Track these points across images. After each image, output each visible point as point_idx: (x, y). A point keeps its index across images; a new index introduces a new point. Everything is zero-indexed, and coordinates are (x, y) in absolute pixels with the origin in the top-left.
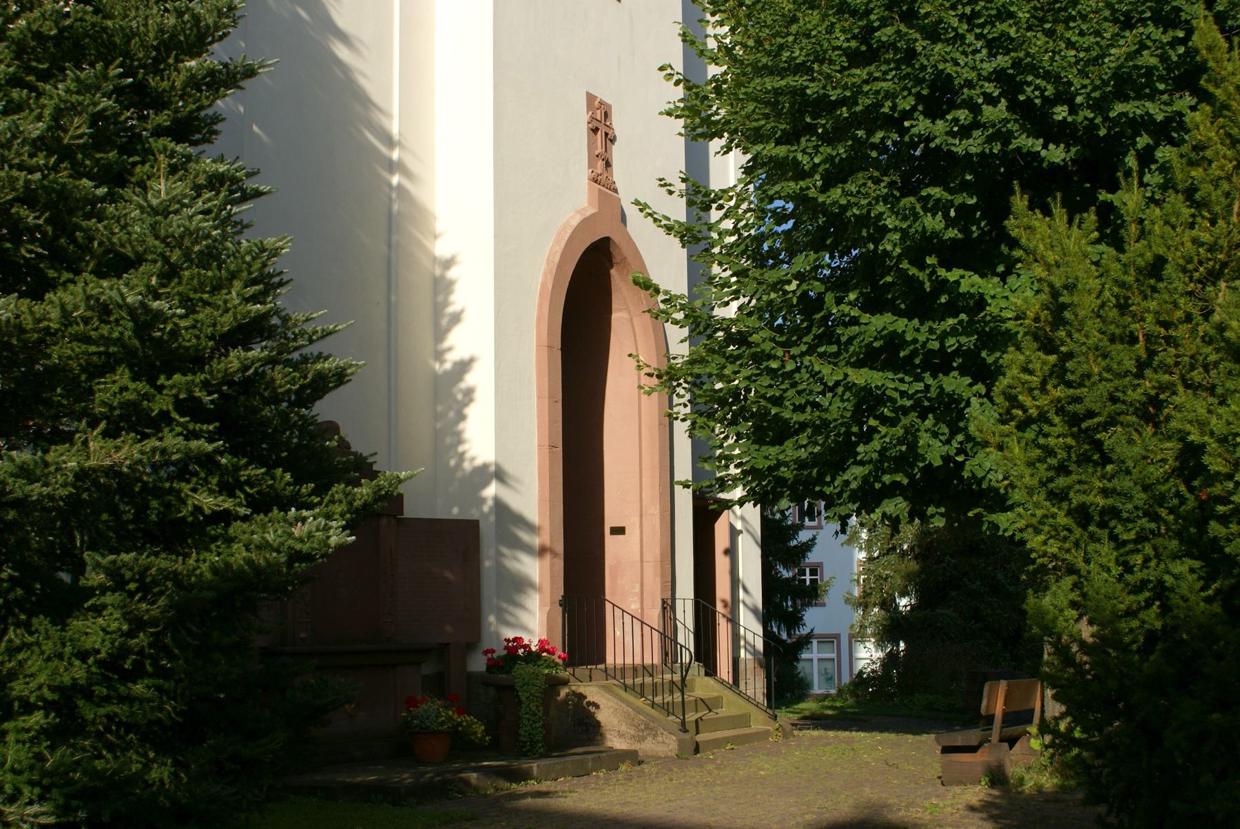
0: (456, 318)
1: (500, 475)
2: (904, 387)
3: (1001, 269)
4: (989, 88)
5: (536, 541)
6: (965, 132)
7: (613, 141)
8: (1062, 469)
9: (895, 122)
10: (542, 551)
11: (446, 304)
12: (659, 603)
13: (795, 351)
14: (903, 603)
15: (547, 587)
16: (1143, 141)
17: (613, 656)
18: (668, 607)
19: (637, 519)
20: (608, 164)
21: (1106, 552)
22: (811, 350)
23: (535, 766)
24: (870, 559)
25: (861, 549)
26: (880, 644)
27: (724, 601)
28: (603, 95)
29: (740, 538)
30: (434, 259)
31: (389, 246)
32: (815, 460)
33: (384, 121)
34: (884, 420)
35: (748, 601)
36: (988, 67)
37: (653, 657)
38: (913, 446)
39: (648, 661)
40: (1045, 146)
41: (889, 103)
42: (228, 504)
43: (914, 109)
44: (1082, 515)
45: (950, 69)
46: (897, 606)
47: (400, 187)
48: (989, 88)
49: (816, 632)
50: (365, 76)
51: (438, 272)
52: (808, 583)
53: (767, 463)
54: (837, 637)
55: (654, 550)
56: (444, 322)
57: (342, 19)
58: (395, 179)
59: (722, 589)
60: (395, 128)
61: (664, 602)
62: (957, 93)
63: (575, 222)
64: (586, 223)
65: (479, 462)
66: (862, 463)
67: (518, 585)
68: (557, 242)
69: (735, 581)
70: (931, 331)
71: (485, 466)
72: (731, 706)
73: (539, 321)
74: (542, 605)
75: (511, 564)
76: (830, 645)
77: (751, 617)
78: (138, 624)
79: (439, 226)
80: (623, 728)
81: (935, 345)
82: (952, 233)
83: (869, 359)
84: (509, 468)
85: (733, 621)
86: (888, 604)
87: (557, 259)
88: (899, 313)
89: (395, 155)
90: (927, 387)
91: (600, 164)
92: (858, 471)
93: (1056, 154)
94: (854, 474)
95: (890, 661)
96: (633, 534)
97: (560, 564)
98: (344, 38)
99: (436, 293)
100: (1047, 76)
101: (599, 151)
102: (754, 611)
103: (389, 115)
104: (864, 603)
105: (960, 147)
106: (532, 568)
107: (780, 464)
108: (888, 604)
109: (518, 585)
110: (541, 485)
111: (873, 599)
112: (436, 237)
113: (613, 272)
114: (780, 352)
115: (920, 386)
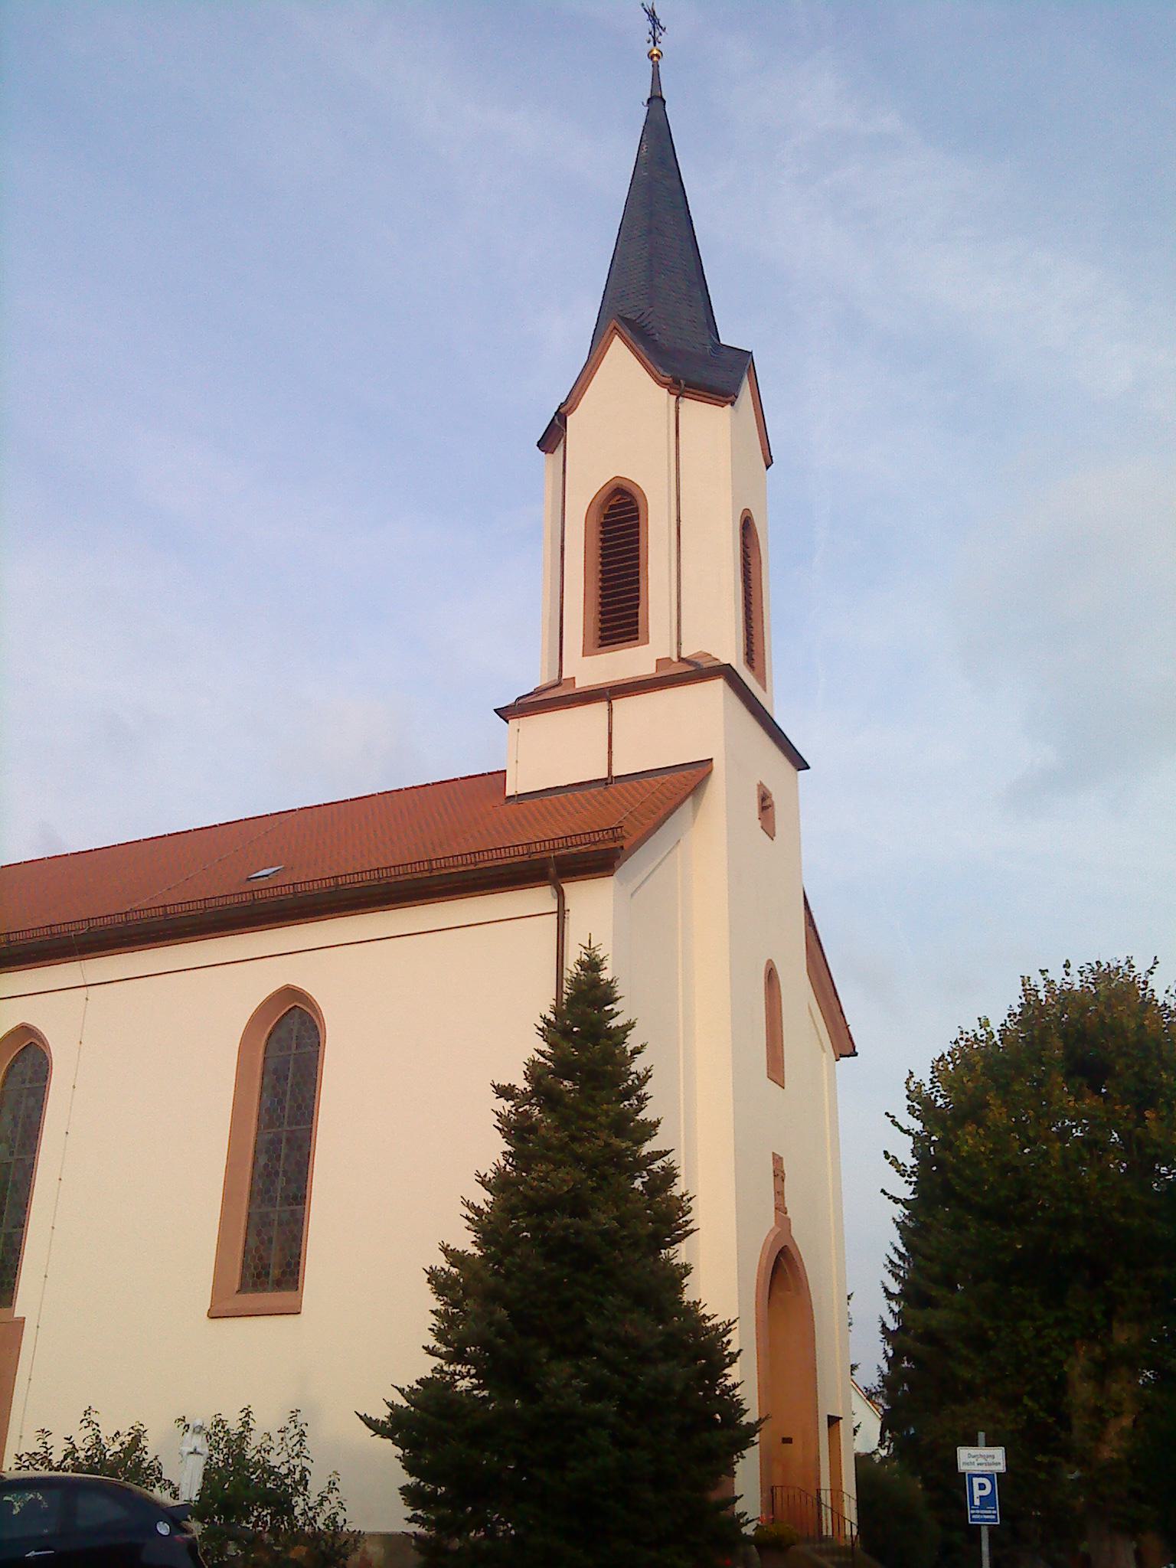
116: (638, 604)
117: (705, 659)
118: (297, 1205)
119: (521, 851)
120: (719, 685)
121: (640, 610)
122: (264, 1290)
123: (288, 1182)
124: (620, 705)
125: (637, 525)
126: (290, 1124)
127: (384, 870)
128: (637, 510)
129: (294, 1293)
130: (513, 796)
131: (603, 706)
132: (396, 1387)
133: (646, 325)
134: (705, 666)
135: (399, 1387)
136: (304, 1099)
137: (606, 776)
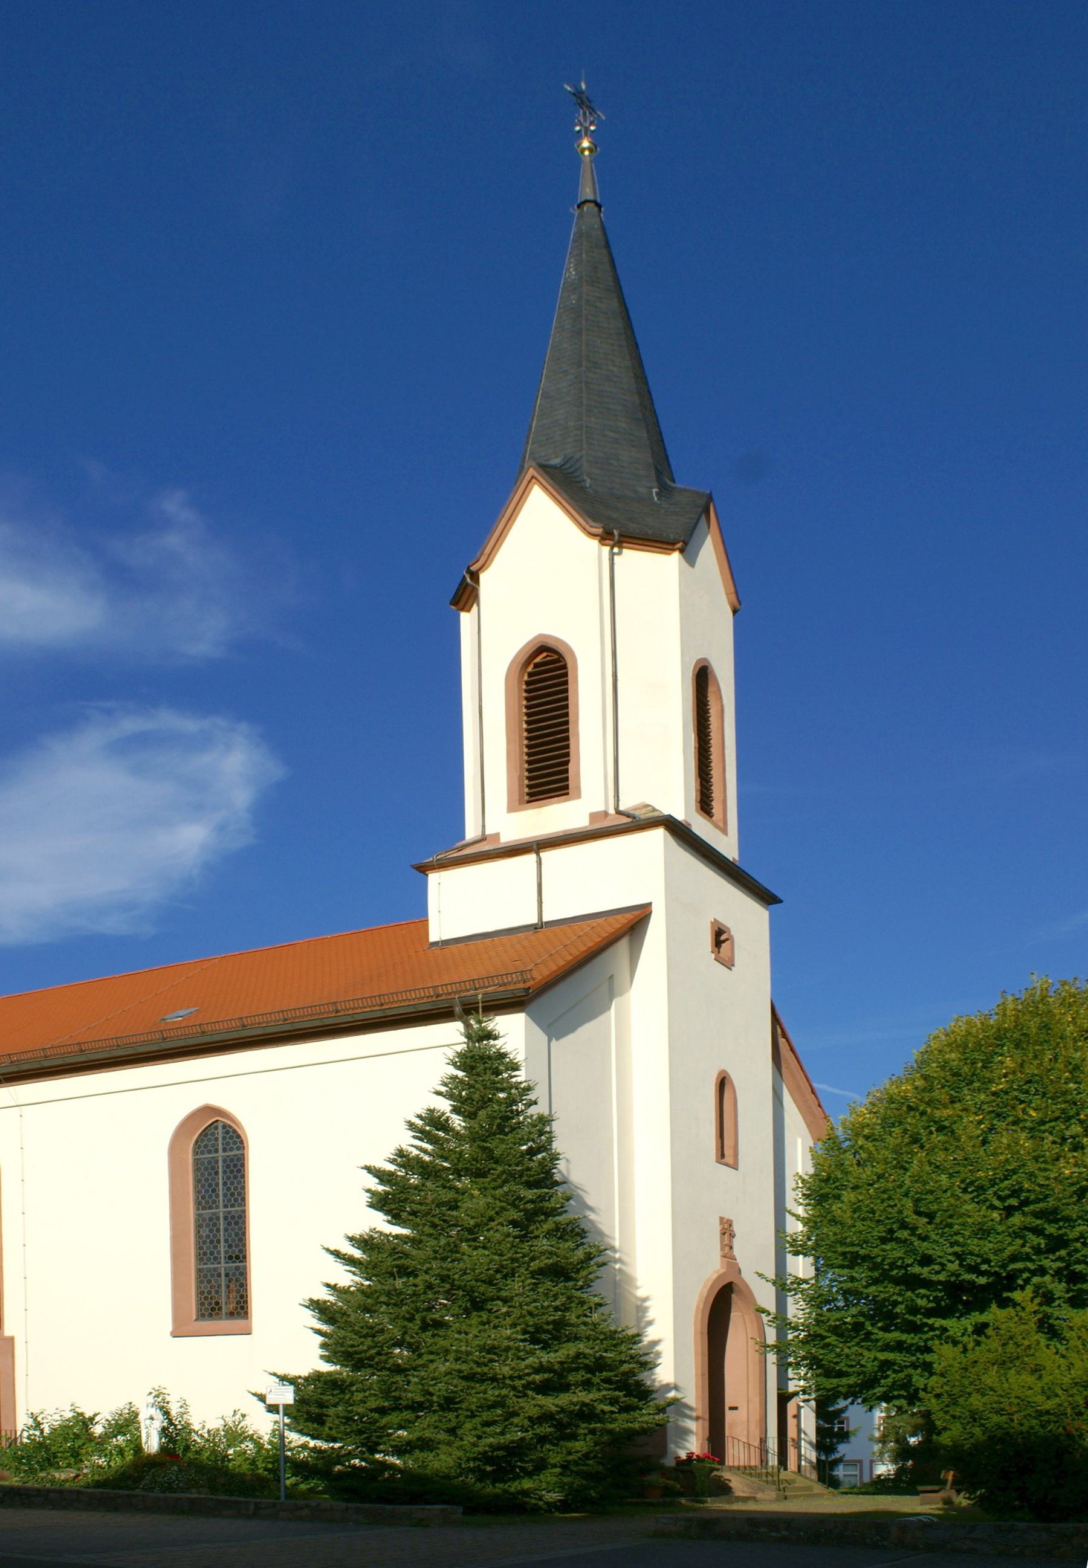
0: (650, 1323)
1: (676, 1388)
2: (906, 1359)
3: (957, 1315)
4: (950, 1258)
5: (694, 1414)
6: (938, 1273)
7: (733, 1237)
8: (947, 1406)
9: (905, 1267)
10: (697, 1418)
11: (643, 1317)
12: (758, 1440)
13: (848, 1345)
14: (913, 1440)
15: (700, 1433)
16: (1025, 1275)
17: (729, 1461)
18: (763, 1441)
19: (746, 1404)
20: (731, 1248)
21: (958, 1425)
22: (858, 1344)
23: (709, 1499)
24: (889, 1417)
25: (882, 1412)
26: (894, 1461)
27: (793, 1440)
28: (727, 1216)
29: (802, 1410)
30: (637, 1298)
31: (615, 1294)
32: (856, 1385)
33: (611, 1242)
34: (895, 1371)
35: (806, 1438)
36: (950, 1250)
37: (755, 1462)
38: (910, 1381)
39: (753, 1464)
40: (977, 1277)
41: (900, 1261)
42: (613, 1409)
43: (913, 1263)
44: (954, 1417)
45: (930, 1252)
46: (908, 1442)
47: (620, 1269)
48: (950, 1258)
49: (846, 1458)
50: (600, 1223)
51: (639, 1303)
52: (836, 1429)
53: (832, 1386)
54: (860, 1462)
55: (756, 1416)
56: (643, 1324)
57: (590, 1201)
58: (617, 1266)
59: (792, 1432)
60: (617, 1244)
61: (761, 1439)
62: (935, 1260)
63: (715, 1276)
64: (720, 1277)
65: (664, 1382)
66: (883, 1386)
67: (685, 1432)
68: (704, 1287)
69: (799, 1430)
70: (921, 1338)
71: (668, 1385)
72: (800, 1482)
73: (695, 1322)
74: (697, 1440)
75: (681, 1423)
76: (854, 1467)
77: (808, 1446)
78: (596, 1444)
79: (639, 1283)
80: (745, 1489)
81: (922, 1344)
82: (931, 1305)
83: (886, 1348)
84: (680, 1384)
85: (798, 1447)
86: (901, 1441)
87: (705, 1294)
88: (902, 1332)
89: (617, 1255)
90: (918, 1358)
91: (727, 1249)
92: (881, 1389)
93: (982, 1281)
94: (879, 1391)
95: (900, 1472)
96: (742, 1412)
97: (707, 1424)
98: (591, 1209)
99: (638, 1312)
100: (977, 1256)
101: (726, 1242)
102: (810, 1443)
103: (614, 1239)
104: (883, 1440)
105: (935, 1278)
106: (692, 1425)
107: (839, 1386)
108: (901, 1441)
109: (685, 1432)
110: (697, 1391)
111: (890, 1438)
112: (637, 1288)
113: (733, 1296)
114: (841, 1345)
115: (914, 1358)
116: (569, 761)
117: (644, 811)
118: (240, 1262)
119: (413, 994)
120: (659, 834)
121: (571, 766)
122: (221, 1319)
123: (230, 1246)
124: (545, 855)
125: (566, 683)
126: (225, 1206)
127: (408, 993)
128: (565, 667)
129: (244, 1321)
130: (438, 942)
131: (532, 858)
132: (275, 1374)
133: (574, 472)
134: (642, 817)
135: (279, 1374)
136: (236, 1188)
137: (534, 920)
